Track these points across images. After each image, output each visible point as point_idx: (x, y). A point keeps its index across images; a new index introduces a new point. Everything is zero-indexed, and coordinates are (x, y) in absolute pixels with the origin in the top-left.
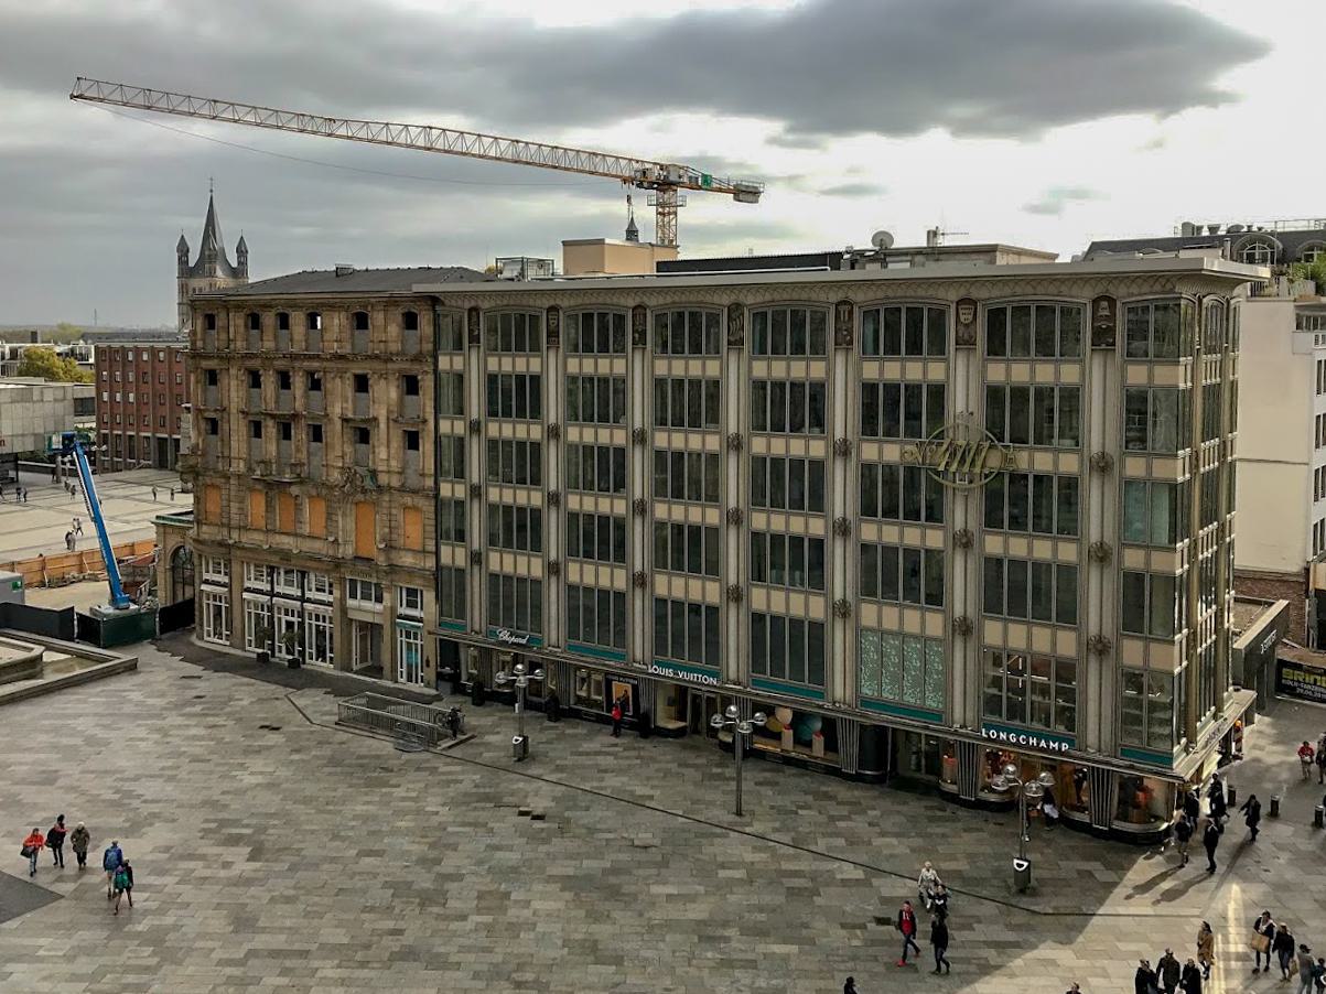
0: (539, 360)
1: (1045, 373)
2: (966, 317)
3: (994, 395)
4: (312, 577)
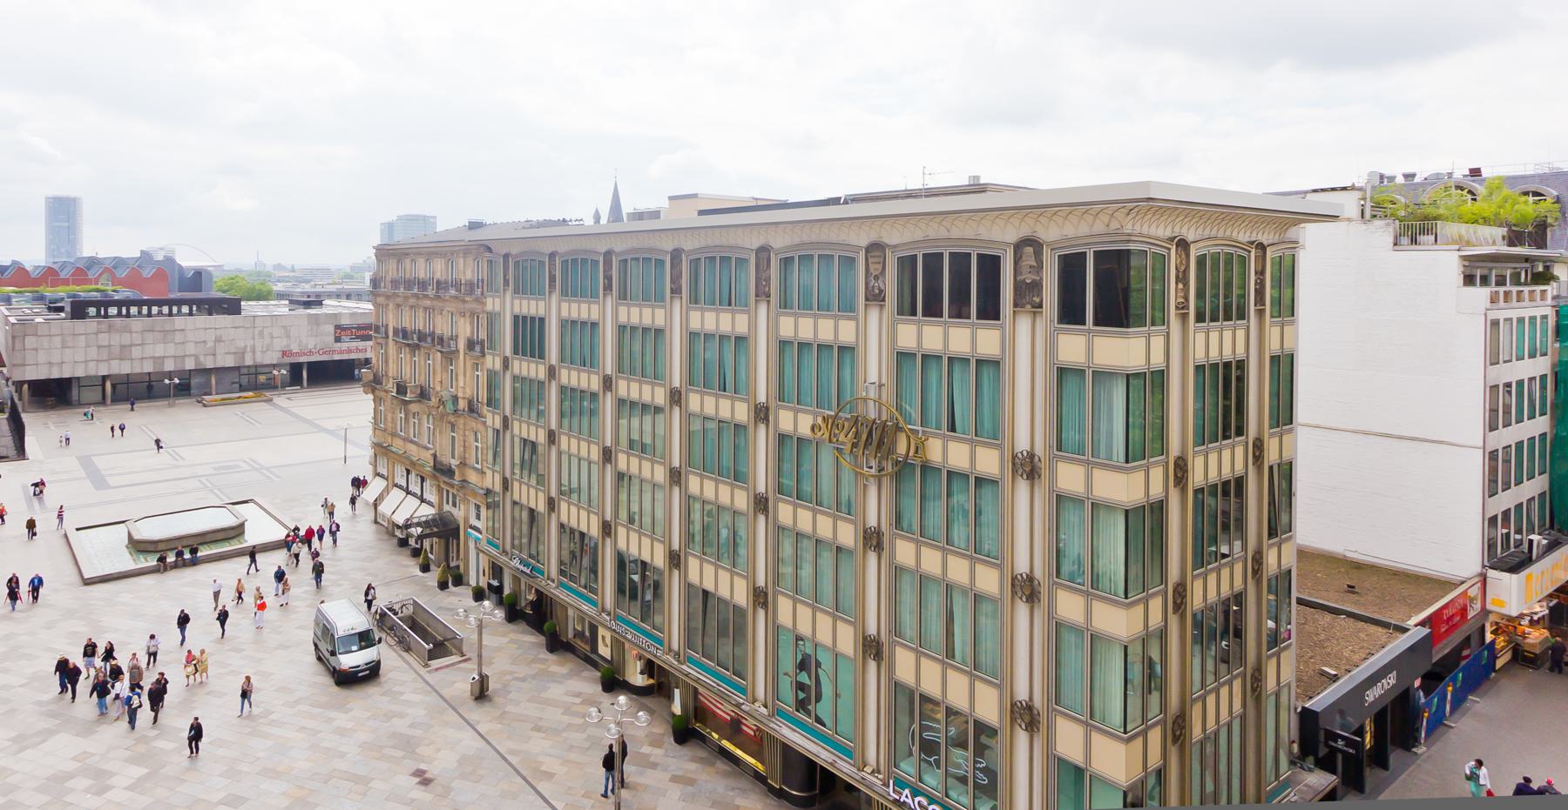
3: (903, 358)
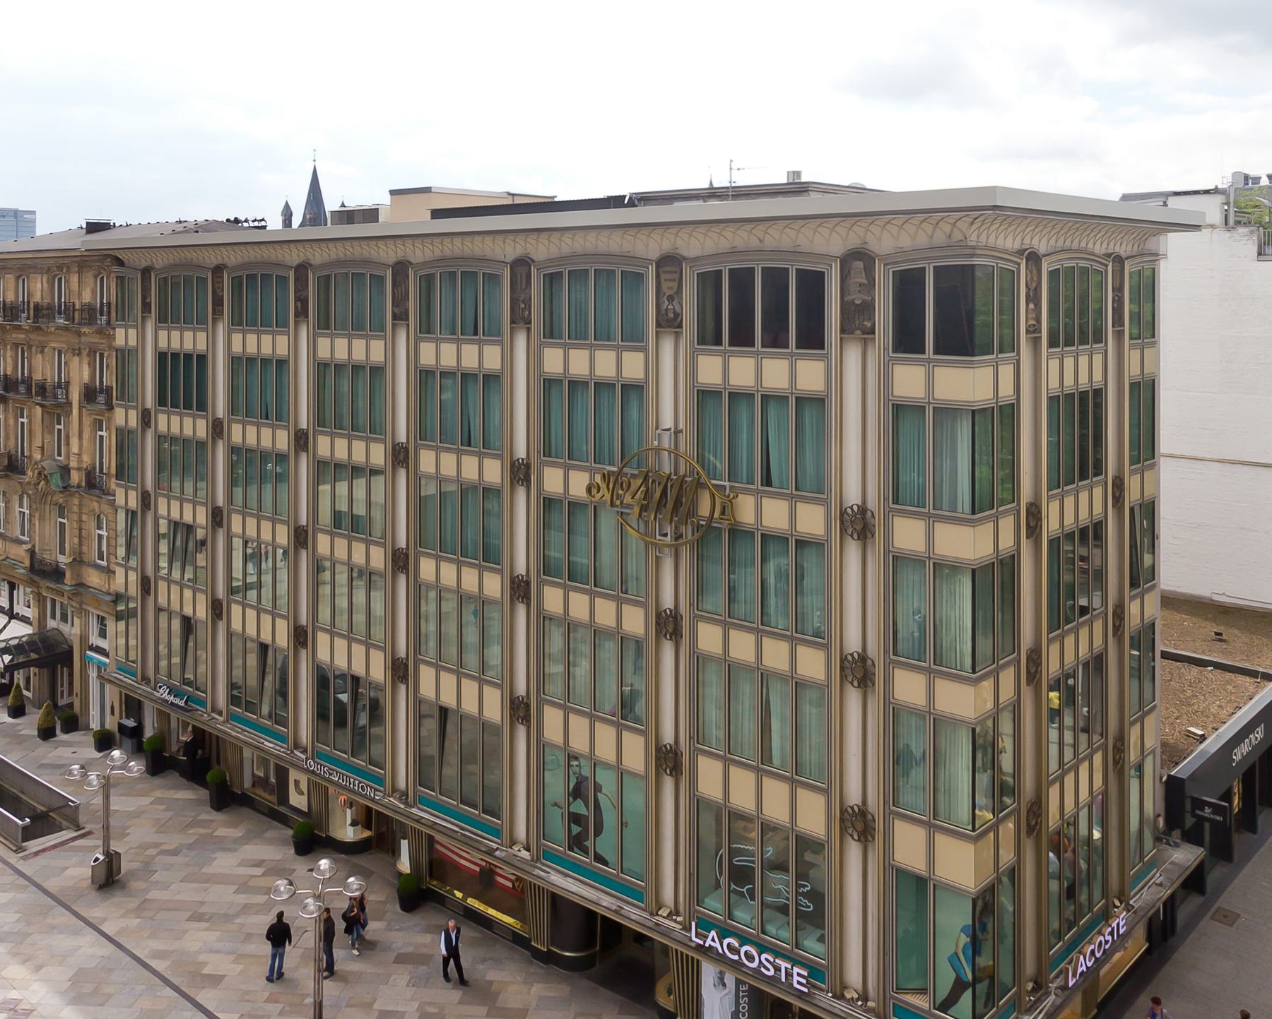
0: (497, 349)
1: (470, 356)
2: (671, 284)
3: (705, 397)
4: (21, 588)
